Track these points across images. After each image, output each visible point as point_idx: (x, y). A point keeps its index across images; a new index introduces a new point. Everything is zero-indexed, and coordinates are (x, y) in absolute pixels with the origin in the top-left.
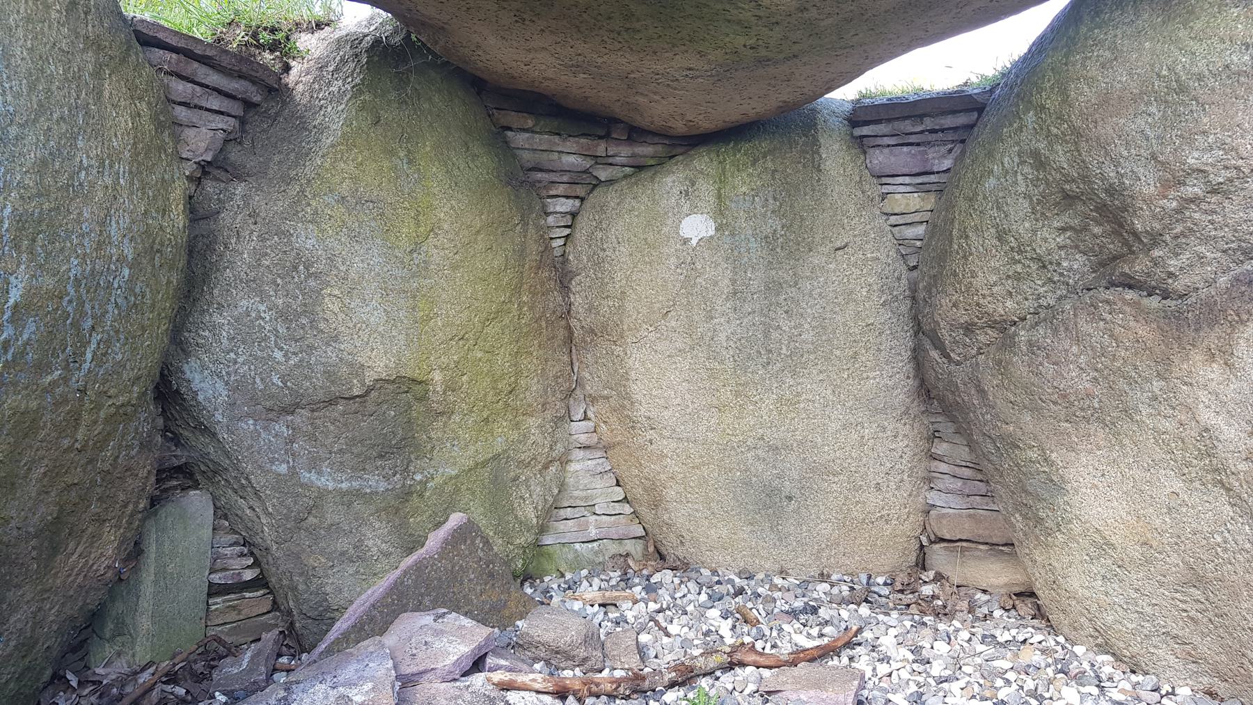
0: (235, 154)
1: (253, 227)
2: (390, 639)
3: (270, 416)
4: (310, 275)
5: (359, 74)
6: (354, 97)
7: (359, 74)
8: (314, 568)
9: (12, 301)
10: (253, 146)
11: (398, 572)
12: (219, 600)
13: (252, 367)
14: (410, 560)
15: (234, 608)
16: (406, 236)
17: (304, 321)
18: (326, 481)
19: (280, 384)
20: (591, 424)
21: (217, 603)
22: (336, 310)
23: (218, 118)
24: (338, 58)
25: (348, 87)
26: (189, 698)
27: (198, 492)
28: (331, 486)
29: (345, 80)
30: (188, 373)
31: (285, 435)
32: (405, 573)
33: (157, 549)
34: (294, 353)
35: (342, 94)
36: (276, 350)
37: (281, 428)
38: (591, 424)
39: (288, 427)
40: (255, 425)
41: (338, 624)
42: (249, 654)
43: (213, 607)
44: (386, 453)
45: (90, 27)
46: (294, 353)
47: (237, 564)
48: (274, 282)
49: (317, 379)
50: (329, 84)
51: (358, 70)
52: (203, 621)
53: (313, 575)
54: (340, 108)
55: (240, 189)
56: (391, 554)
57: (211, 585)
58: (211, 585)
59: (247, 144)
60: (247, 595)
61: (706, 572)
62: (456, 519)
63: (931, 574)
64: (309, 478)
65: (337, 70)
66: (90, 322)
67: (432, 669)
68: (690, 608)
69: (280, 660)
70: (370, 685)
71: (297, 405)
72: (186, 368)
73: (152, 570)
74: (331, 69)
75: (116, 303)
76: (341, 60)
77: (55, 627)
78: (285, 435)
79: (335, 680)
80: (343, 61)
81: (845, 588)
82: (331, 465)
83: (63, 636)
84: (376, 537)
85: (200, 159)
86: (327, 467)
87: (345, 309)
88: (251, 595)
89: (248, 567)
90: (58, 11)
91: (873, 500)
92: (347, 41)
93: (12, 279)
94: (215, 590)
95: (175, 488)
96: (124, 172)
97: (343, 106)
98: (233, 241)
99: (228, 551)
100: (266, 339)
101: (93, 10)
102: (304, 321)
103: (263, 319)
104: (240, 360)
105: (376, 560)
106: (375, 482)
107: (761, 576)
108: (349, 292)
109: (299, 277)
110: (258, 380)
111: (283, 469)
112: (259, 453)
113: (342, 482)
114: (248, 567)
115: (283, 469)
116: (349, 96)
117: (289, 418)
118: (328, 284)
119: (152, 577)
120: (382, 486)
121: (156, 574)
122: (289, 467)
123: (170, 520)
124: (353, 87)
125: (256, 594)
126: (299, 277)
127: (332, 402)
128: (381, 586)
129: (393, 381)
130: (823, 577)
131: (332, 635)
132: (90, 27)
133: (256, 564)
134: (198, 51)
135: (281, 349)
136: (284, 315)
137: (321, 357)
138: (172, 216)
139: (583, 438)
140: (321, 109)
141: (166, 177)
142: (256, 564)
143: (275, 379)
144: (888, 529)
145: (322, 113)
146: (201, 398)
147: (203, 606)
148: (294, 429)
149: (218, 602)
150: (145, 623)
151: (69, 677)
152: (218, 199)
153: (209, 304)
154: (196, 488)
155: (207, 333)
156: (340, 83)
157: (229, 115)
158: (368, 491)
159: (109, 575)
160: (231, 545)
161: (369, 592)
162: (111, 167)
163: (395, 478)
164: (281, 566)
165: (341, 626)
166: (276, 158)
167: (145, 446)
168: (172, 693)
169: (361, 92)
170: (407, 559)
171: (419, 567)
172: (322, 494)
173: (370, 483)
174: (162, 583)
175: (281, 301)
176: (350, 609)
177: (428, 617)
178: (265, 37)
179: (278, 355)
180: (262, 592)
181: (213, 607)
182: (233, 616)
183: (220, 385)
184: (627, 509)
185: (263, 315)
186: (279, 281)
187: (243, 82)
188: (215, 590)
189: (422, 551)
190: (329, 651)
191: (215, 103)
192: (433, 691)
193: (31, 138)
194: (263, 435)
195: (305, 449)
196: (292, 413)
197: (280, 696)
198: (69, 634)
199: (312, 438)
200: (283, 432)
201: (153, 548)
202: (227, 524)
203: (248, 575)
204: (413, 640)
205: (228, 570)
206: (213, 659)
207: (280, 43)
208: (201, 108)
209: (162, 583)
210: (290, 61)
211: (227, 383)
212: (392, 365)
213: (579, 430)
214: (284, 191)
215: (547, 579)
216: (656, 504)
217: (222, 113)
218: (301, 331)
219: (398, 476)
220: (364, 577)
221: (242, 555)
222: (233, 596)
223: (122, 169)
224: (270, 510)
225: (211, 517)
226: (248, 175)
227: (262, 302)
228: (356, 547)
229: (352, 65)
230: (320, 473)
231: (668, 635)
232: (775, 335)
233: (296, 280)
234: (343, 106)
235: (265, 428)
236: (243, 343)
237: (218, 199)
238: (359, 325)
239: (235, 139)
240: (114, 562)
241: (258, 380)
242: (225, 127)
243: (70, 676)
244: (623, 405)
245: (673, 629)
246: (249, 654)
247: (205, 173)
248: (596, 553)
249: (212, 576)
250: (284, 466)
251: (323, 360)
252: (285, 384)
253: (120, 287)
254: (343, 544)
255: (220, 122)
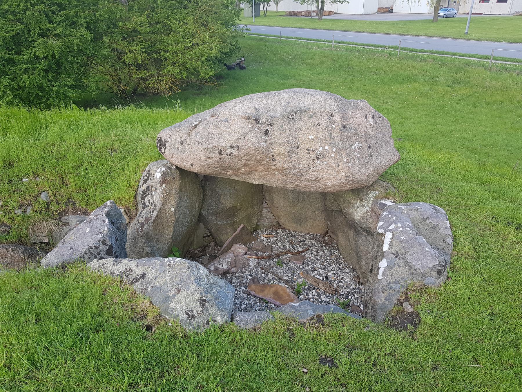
2: (232, 249)
11: (233, 236)
14: (234, 234)
20: (267, 204)
28: (222, 223)
32: (234, 236)
38: (267, 204)
41: (224, 245)
61: (287, 231)
62: (242, 226)
63: (328, 235)
68: (283, 239)
70: (231, 259)
81: (312, 236)
84: (229, 230)
87: (224, 199)
91: (318, 223)
94: (204, 237)
99: (206, 231)
106: (229, 222)
107: (297, 232)
111: (215, 222)
115: (215, 222)
120: (230, 222)
128: (230, 238)
130: (308, 234)
133: (210, 232)
139: (265, 206)
142: (210, 232)
144: (321, 227)
149: (205, 239)
164: (214, 233)
171: (236, 235)
172: (221, 225)
183: (206, 213)
184: (274, 217)
188: (204, 237)
189: (237, 232)
199: (219, 217)
203: (209, 234)
213: (265, 205)
215: (258, 231)
216: (279, 218)
231: (277, 245)
232: (300, 197)
244: (273, 203)
245: (279, 244)
248: (267, 225)
254: (224, 232)
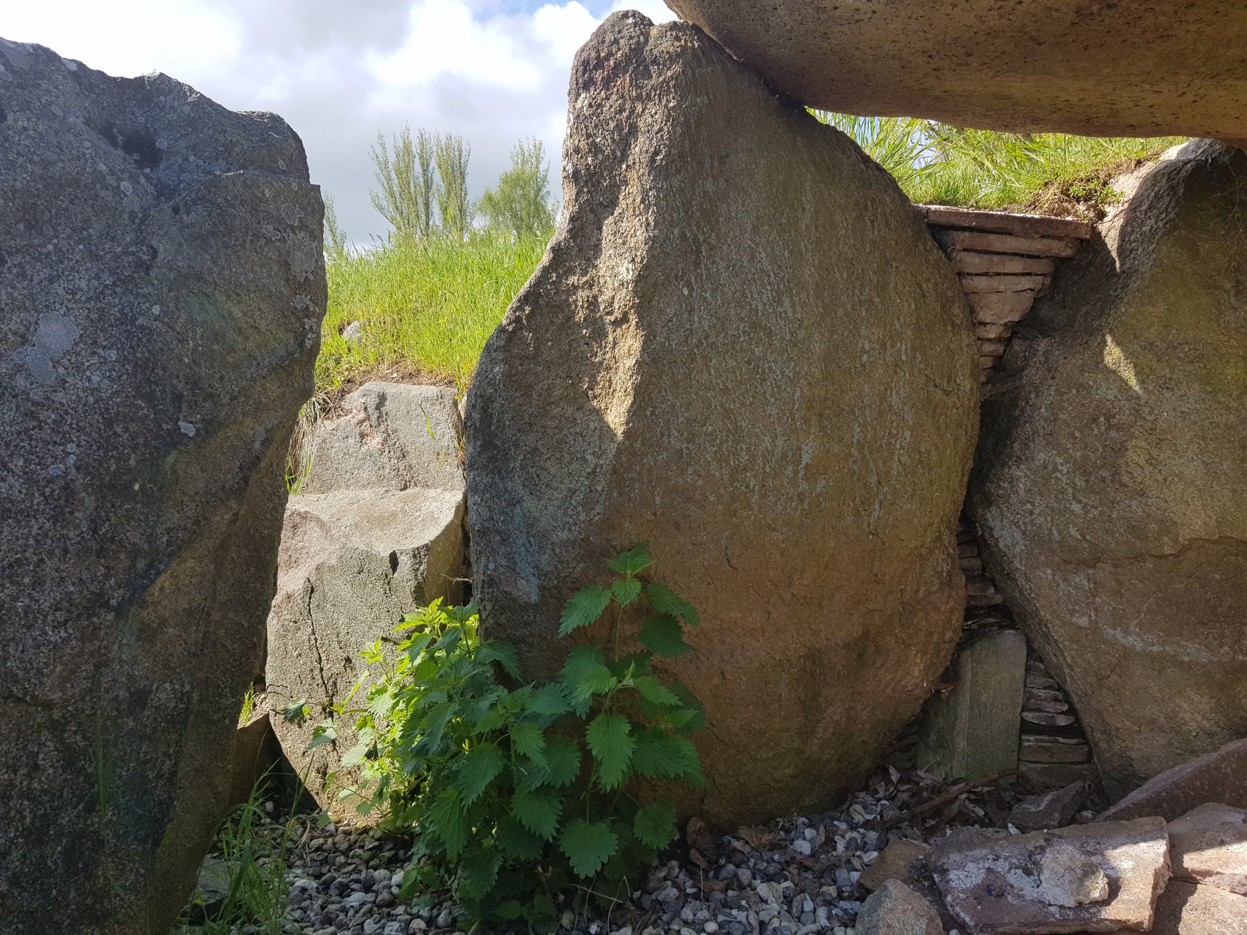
0: (1045, 312)
1: (1050, 382)
3: (1069, 567)
4: (1110, 427)
5: (1173, 208)
6: (1169, 233)
7: (1173, 208)
8: (1118, 729)
9: (804, 463)
10: (1064, 301)
12: (1032, 738)
13: (1049, 519)
15: (1047, 749)
16: (1233, 378)
17: (1105, 473)
18: (1134, 641)
19: (1079, 537)
21: (1028, 741)
22: (1142, 462)
23: (1023, 279)
24: (1153, 194)
25: (1161, 224)
26: (987, 821)
27: (1013, 631)
28: (1139, 646)
29: (1158, 217)
30: (991, 520)
31: (1086, 588)
32: (1223, 759)
33: (972, 678)
34: (1093, 507)
35: (1153, 232)
36: (1074, 503)
37: (1080, 579)
39: (1089, 580)
40: (1053, 575)
42: (1049, 797)
43: (1026, 744)
44: (1209, 621)
45: (876, 232)
46: (1093, 507)
47: (1051, 707)
48: (1072, 435)
49: (1120, 534)
50: (1142, 224)
51: (1173, 204)
52: (1015, 754)
53: (1117, 737)
54: (1151, 248)
55: (1042, 345)
56: (1216, 733)
57: (1023, 721)
58: (1023, 721)
59: (1058, 298)
60: (1061, 740)
64: (1114, 635)
65: (1150, 208)
66: (874, 478)
67: (1218, 873)
69: (1084, 813)
71: (1098, 560)
72: (988, 516)
73: (968, 695)
74: (1144, 208)
75: (899, 461)
76: (1156, 196)
77: (868, 726)
78: (1086, 588)
79: (1098, 846)
80: (1158, 197)
82: (1140, 625)
83: (878, 735)
85: (1006, 320)
86: (1135, 626)
88: (1065, 741)
89: (1063, 713)
90: (844, 228)
92: (1164, 174)
93: (803, 446)
94: (1026, 728)
95: (992, 624)
96: (906, 349)
97: (1154, 245)
98: (1033, 396)
99: (1042, 693)
100: (1063, 491)
101: (879, 217)
102: (1105, 473)
103: (1060, 472)
104: (1037, 511)
105: (1194, 737)
108: (1157, 443)
109: (1099, 429)
110: (1055, 532)
111: (1083, 622)
112: (1057, 603)
113: (1154, 645)
114: (1063, 713)
116: (1160, 234)
117: (1090, 571)
118: (1132, 437)
119: (968, 703)
121: (971, 700)
122: (1091, 621)
123: (984, 653)
124: (1166, 223)
125: (1069, 741)
126: (1099, 429)
127: (1139, 558)
129: (1215, 542)
131: (1123, 803)
132: (876, 232)
134: (989, 225)
135: (1080, 502)
136: (1082, 468)
137: (1124, 511)
138: (958, 381)
140: (1131, 252)
141: (952, 347)
143: (1073, 531)
145: (1132, 256)
146: (1001, 545)
147: (1015, 739)
148: (1095, 583)
149: (1030, 740)
150: (961, 743)
151: (891, 772)
152: (1025, 356)
153: (1010, 458)
154: (1013, 628)
155: (1006, 485)
156: (1153, 221)
157: (1036, 275)
158: (1186, 659)
159: (917, 692)
160: (1045, 688)
161: (1177, 769)
162: (893, 347)
163: (1222, 650)
165: (1136, 796)
166: (1084, 310)
167: (947, 583)
168: (973, 811)
169: (1175, 228)
170: (1230, 744)
173: (1188, 651)
174: (977, 710)
175: (1079, 454)
176: (1150, 782)
177: (1237, 815)
178: (1077, 189)
179: (1076, 507)
180: (1075, 741)
181: (1026, 744)
182: (1045, 757)
183: (1018, 535)
185: (1060, 467)
186: (1077, 434)
187: (1045, 241)
190: (1116, 817)
191: (1016, 266)
192: (1216, 897)
193: (817, 337)
194: (1062, 586)
195: (1109, 605)
196: (1094, 567)
197: (1038, 844)
198: (885, 735)
200: (1084, 585)
201: (969, 676)
202: (1042, 667)
203: (1062, 721)
204: (1207, 834)
205: (1042, 711)
206: (1020, 793)
207: (1096, 191)
208: (998, 274)
209: (977, 710)
210: (1106, 206)
211: (1024, 533)
212: (1213, 523)
214: (1086, 343)
217: (1030, 274)
218: (1101, 484)
219: (1226, 648)
220: (1179, 751)
221: (1056, 699)
222: (1045, 738)
223: (904, 347)
224: (1069, 660)
225: (1024, 659)
226: (1055, 330)
227: (1060, 455)
228: (1168, 717)
229: (1167, 199)
230: (1126, 632)
233: (1096, 432)
234: (1154, 245)
235: (1065, 580)
236: (1040, 495)
237: (1025, 356)
238: (1170, 478)
239: (1045, 296)
240: (922, 681)
241: (1055, 532)
242: (1032, 287)
243: (892, 770)
246: (1049, 797)
247: (1014, 334)
249: (1025, 714)
250: (1085, 619)
251: (1128, 515)
252: (1083, 536)
253: (902, 447)
255: (1026, 283)
